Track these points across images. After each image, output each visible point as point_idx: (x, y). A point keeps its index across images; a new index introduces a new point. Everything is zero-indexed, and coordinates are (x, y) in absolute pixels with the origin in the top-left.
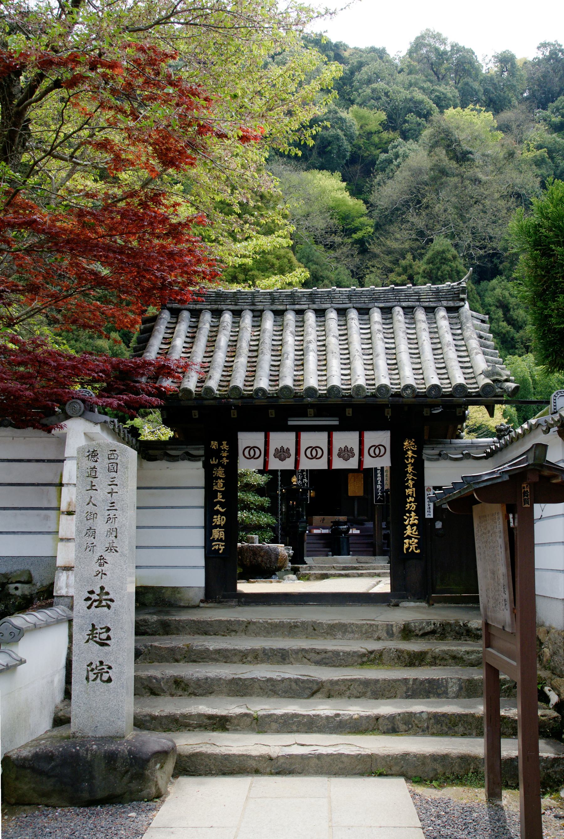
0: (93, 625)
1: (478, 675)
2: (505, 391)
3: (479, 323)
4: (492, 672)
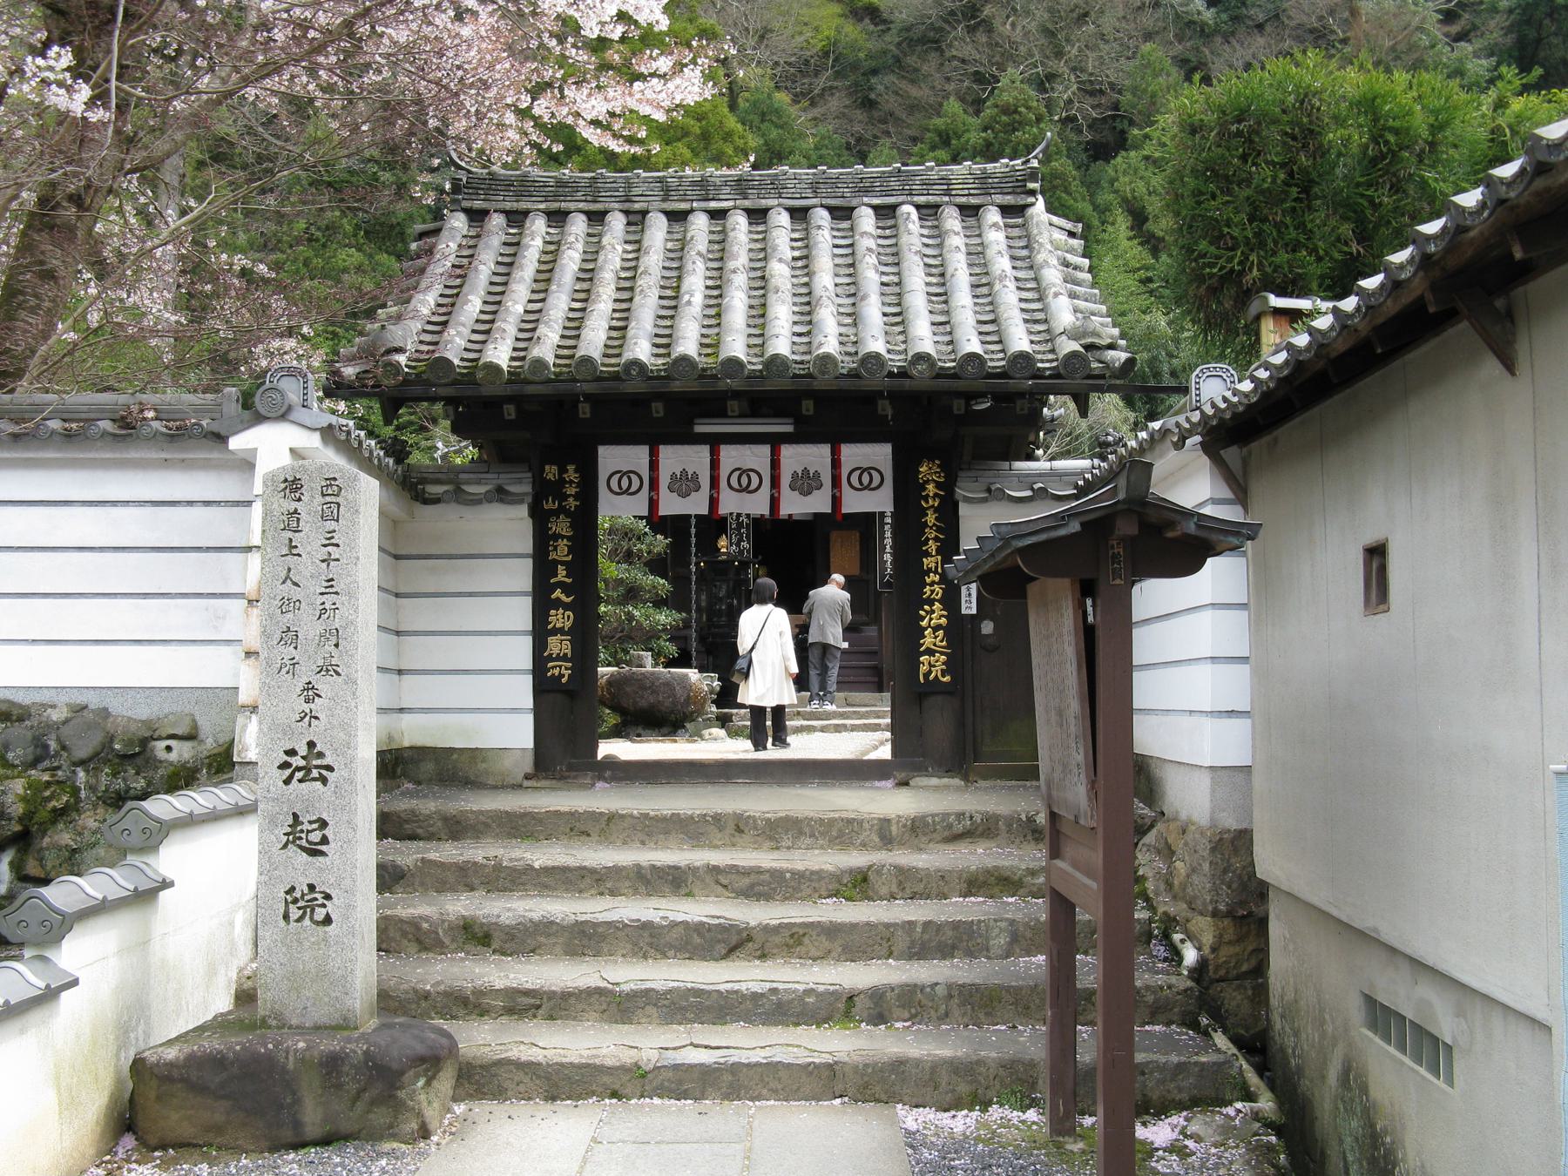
0: (295, 816)
1: (1039, 909)
2: (1108, 367)
3: (1063, 237)
4: (1062, 907)
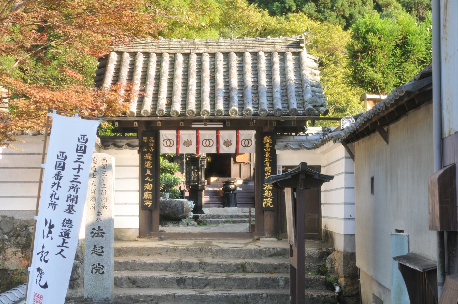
0: (95, 246)
